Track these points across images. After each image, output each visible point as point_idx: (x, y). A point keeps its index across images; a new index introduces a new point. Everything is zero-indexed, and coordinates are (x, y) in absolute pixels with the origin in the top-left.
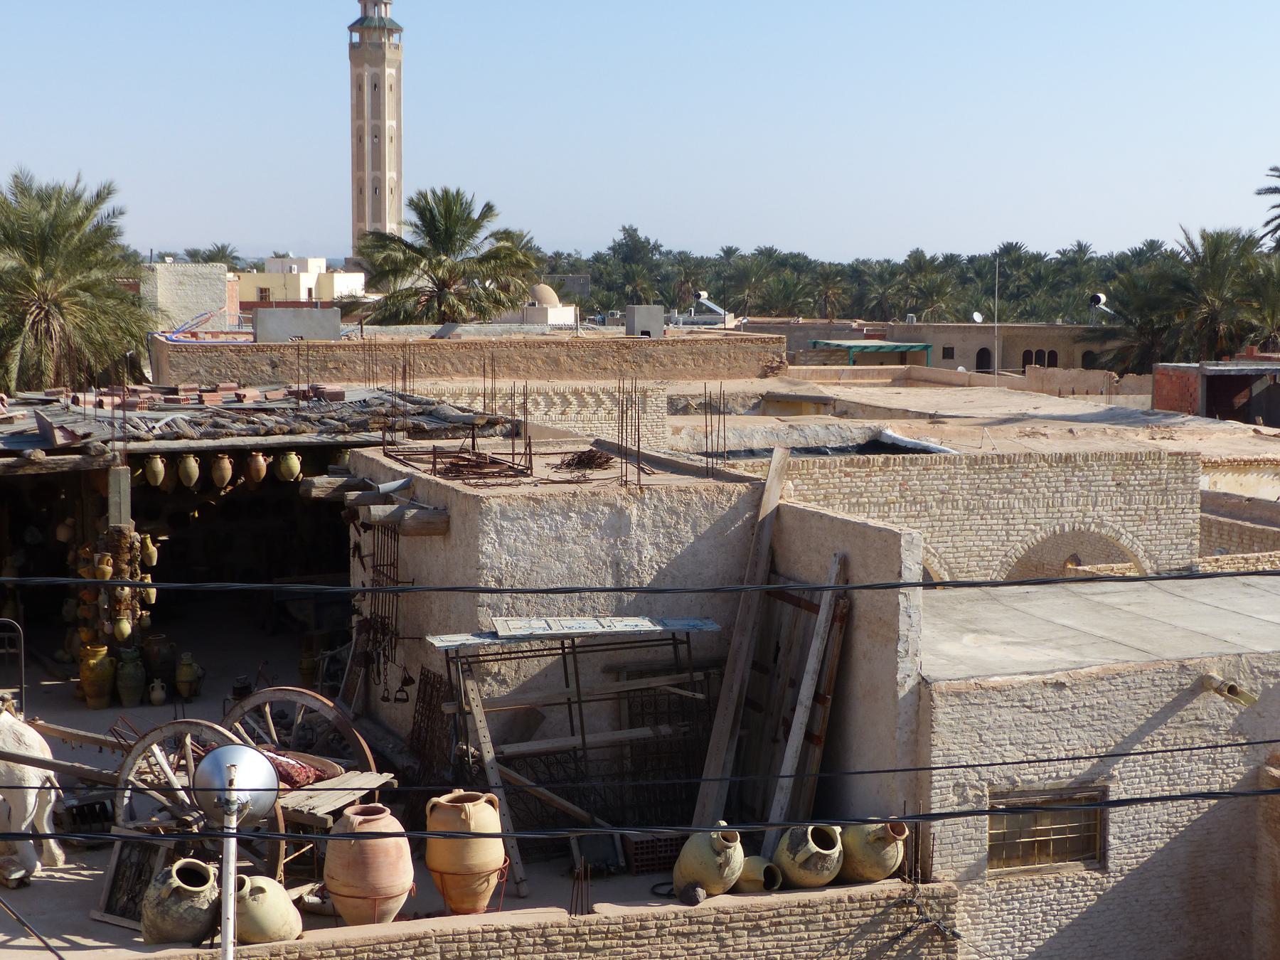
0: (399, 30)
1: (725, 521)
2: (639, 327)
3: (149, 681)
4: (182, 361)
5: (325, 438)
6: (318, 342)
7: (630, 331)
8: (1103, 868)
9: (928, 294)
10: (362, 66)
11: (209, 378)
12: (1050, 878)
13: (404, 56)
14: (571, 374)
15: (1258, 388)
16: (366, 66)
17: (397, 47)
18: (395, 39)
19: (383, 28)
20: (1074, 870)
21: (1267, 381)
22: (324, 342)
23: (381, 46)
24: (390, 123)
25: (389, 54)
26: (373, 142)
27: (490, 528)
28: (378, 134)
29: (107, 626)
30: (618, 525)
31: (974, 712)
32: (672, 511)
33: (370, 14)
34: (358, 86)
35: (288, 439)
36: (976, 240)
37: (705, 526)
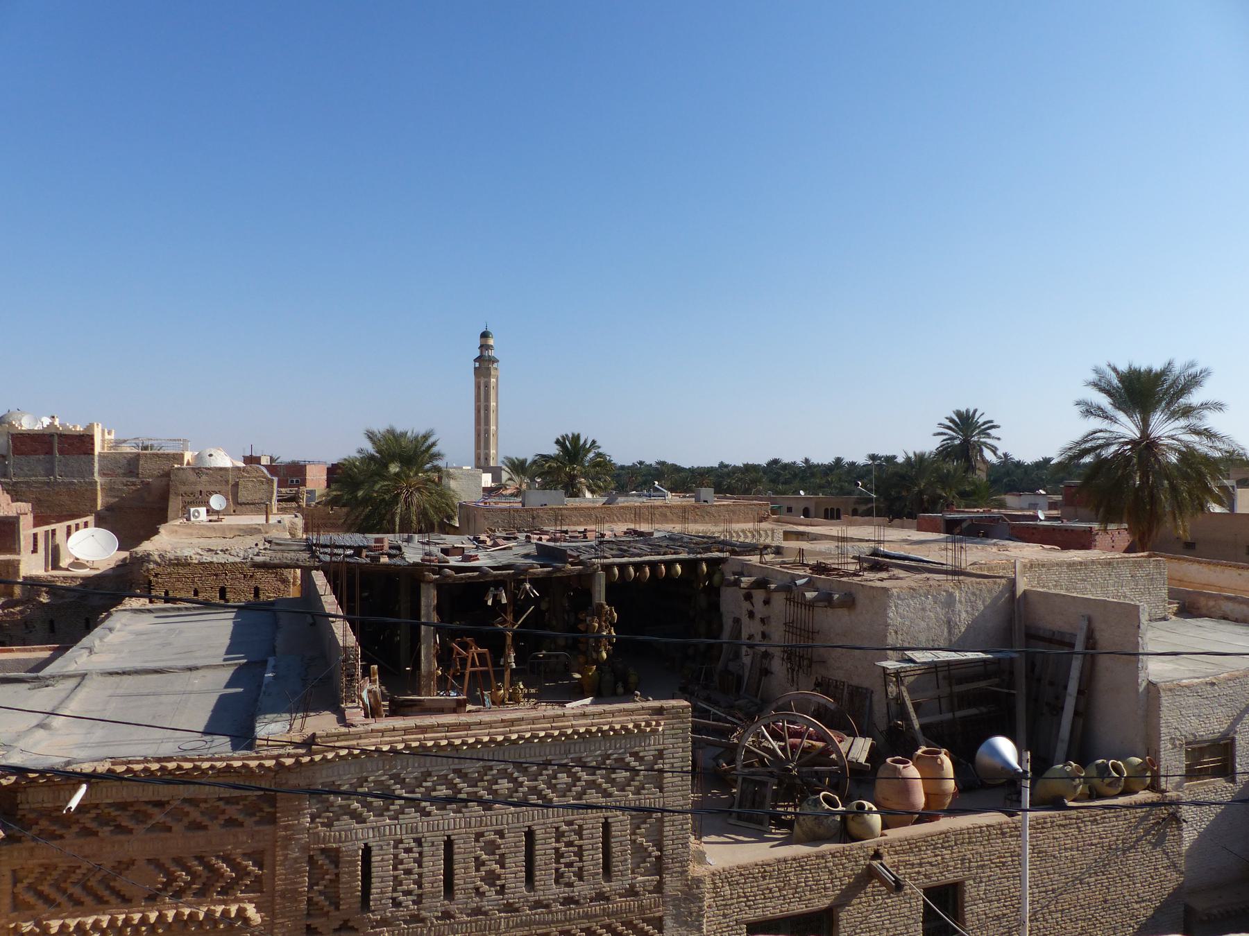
0: (497, 361)
1: (997, 598)
2: (702, 498)
3: (616, 683)
5: (692, 556)
7: (697, 500)
8: (1233, 781)
9: (755, 482)
12: (1211, 787)
13: (500, 374)
14: (672, 521)
15: (964, 525)
18: (495, 365)
20: (1220, 782)
21: (969, 522)
23: (489, 369)
24: (493, 404)
27: (892, 604)
28: (487, 408)
29: (595, 655)
30: (950, 602)
31: (1178, 699)
32: (974, 594)
34: (478, 387)
35: (675, 556)
36: (761, 459)
37: (988, 601)
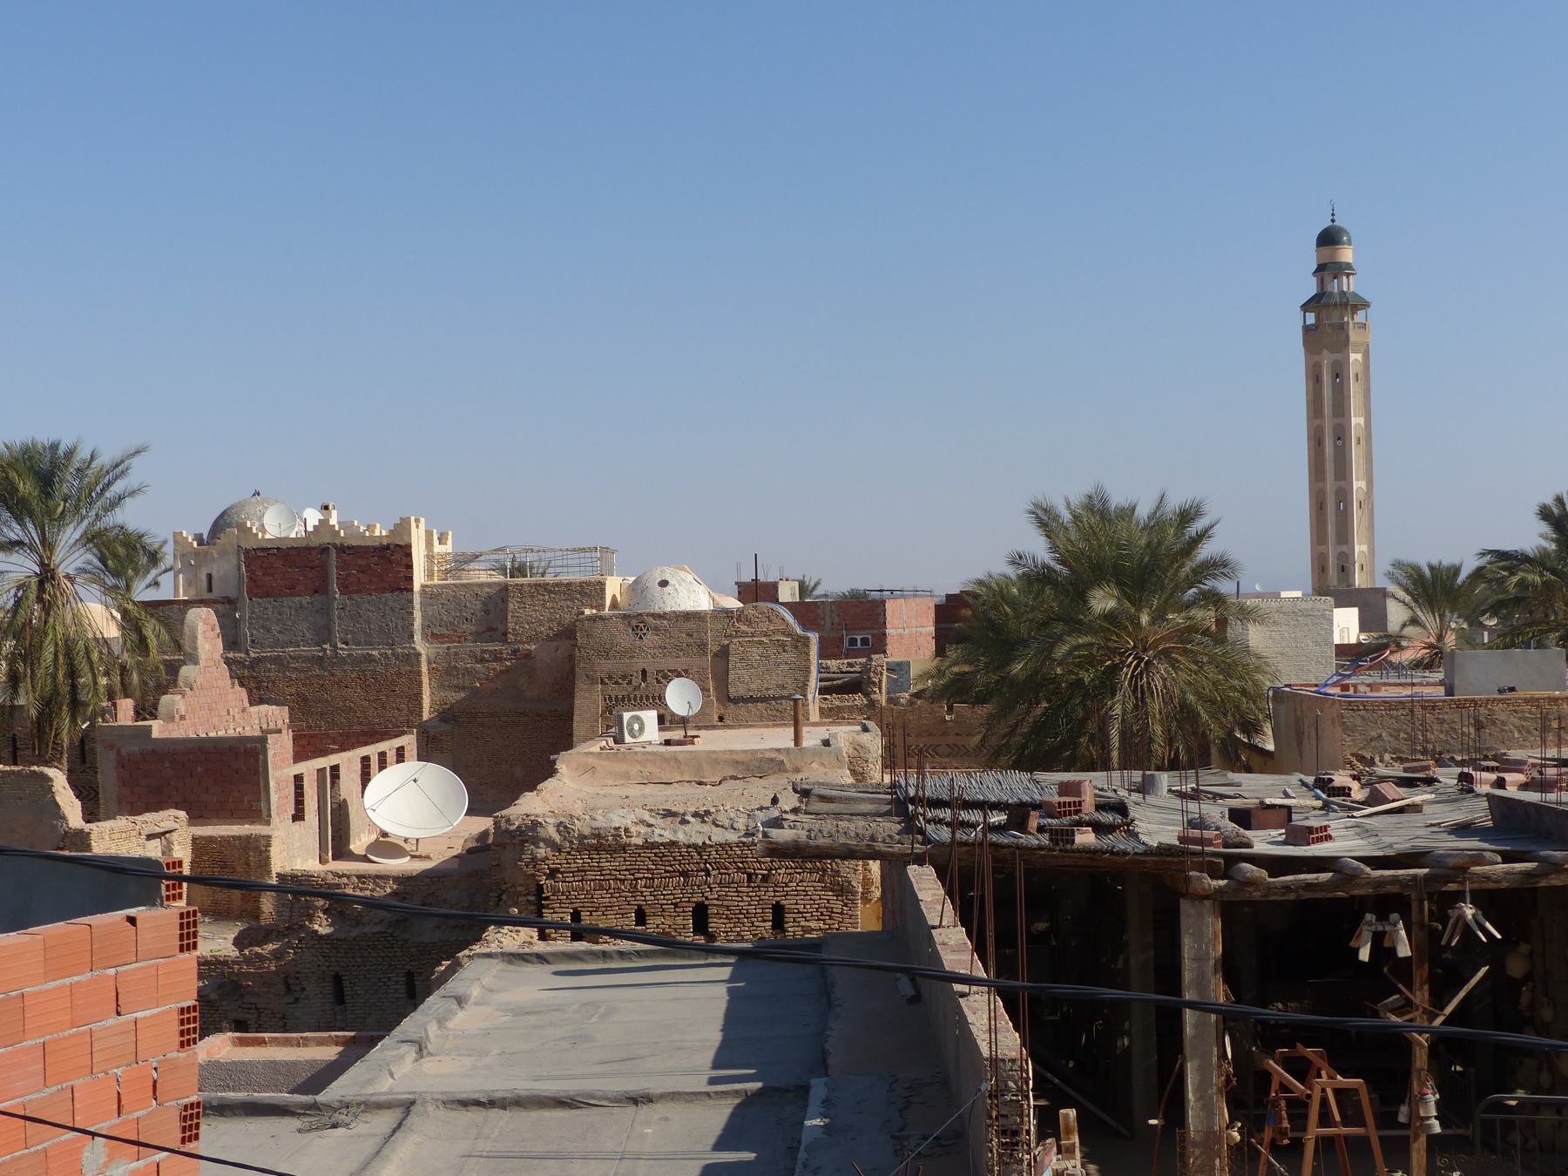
0: (1365, 305)
4: (1358, 721)
6: (1537, 694)
10: (1319, 352)
11: (1394, 744)
13: (1373, 337)
16: (1325, 352)
17: (1363, 326)
18: (1360, 317)
19: (1346, 304)
22: (1546, 694)
23: (1342, 328)
24: (1357, 421)
25: (1354, 336)
26: (1335, 446)
28: (1342, 434)
33: (1329, 289)
34: (1315, 378)
